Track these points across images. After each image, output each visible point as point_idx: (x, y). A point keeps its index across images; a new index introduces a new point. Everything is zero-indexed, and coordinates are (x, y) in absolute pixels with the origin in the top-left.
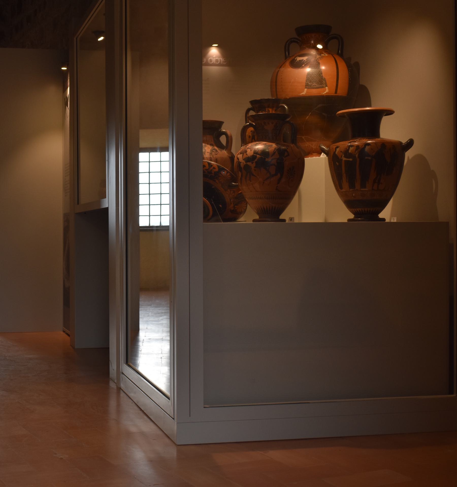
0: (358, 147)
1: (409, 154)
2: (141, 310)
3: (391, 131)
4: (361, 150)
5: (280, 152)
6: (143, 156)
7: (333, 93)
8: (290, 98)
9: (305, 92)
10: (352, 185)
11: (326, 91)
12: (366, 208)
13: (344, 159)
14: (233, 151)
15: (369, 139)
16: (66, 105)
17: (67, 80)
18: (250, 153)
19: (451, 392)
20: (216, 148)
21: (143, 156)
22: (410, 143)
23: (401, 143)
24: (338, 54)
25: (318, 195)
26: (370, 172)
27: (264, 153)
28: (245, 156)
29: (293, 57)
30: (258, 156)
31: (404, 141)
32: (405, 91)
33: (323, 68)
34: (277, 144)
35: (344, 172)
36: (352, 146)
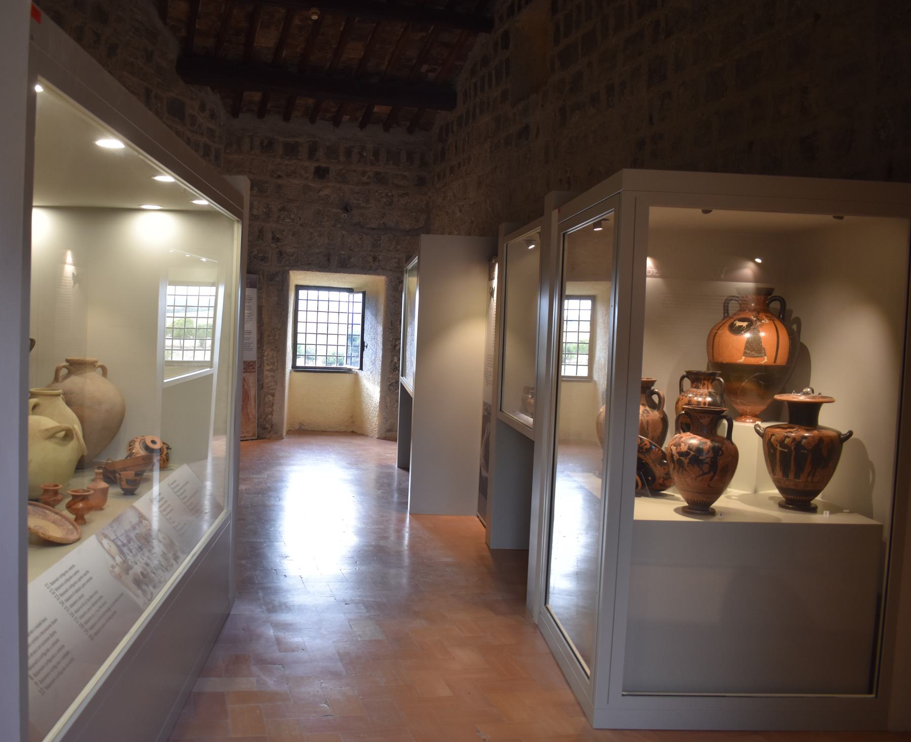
0: (794, 439)
1: (846, 445)
2: (562, 472)
3: (830, 420)
4: (797, 443)
5: (713, 448)
6: (566, 301)
7: (771, 363)
8: (727, 364)
9: (742, 360)
10: (785, 473)
11: (765, 361)
12: (798, 498)
13: (779, 448)
14: (665, 409)
15: (807, 431)
16: (492, 294)
17: (494, 270)
18: (684, 448)
19: (870, 692)
20: (647, 408)
21: (566, 301)
22: (851, 433)
23: (839, 434)
24: (778, 318)
25: (752, 492)
26: (804, 463)
27: (699, 450)
28: (679, 450)
29: (732, 320)
30: (692, 453)
31: (844, 431)
32: (847, 379)
33: (762, 334)
34: (712, 441)
35: (780, 458)
36: (788, 437)
